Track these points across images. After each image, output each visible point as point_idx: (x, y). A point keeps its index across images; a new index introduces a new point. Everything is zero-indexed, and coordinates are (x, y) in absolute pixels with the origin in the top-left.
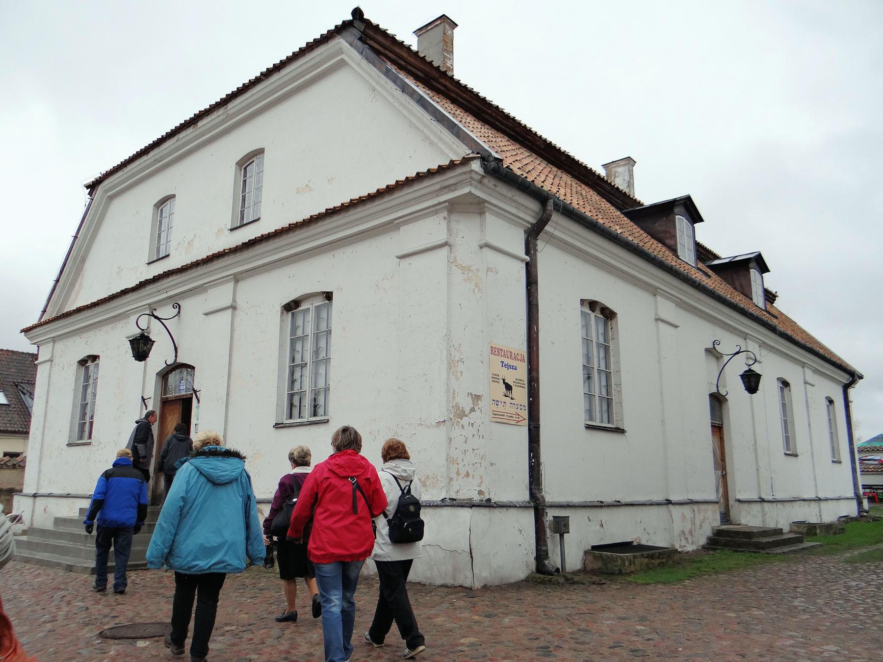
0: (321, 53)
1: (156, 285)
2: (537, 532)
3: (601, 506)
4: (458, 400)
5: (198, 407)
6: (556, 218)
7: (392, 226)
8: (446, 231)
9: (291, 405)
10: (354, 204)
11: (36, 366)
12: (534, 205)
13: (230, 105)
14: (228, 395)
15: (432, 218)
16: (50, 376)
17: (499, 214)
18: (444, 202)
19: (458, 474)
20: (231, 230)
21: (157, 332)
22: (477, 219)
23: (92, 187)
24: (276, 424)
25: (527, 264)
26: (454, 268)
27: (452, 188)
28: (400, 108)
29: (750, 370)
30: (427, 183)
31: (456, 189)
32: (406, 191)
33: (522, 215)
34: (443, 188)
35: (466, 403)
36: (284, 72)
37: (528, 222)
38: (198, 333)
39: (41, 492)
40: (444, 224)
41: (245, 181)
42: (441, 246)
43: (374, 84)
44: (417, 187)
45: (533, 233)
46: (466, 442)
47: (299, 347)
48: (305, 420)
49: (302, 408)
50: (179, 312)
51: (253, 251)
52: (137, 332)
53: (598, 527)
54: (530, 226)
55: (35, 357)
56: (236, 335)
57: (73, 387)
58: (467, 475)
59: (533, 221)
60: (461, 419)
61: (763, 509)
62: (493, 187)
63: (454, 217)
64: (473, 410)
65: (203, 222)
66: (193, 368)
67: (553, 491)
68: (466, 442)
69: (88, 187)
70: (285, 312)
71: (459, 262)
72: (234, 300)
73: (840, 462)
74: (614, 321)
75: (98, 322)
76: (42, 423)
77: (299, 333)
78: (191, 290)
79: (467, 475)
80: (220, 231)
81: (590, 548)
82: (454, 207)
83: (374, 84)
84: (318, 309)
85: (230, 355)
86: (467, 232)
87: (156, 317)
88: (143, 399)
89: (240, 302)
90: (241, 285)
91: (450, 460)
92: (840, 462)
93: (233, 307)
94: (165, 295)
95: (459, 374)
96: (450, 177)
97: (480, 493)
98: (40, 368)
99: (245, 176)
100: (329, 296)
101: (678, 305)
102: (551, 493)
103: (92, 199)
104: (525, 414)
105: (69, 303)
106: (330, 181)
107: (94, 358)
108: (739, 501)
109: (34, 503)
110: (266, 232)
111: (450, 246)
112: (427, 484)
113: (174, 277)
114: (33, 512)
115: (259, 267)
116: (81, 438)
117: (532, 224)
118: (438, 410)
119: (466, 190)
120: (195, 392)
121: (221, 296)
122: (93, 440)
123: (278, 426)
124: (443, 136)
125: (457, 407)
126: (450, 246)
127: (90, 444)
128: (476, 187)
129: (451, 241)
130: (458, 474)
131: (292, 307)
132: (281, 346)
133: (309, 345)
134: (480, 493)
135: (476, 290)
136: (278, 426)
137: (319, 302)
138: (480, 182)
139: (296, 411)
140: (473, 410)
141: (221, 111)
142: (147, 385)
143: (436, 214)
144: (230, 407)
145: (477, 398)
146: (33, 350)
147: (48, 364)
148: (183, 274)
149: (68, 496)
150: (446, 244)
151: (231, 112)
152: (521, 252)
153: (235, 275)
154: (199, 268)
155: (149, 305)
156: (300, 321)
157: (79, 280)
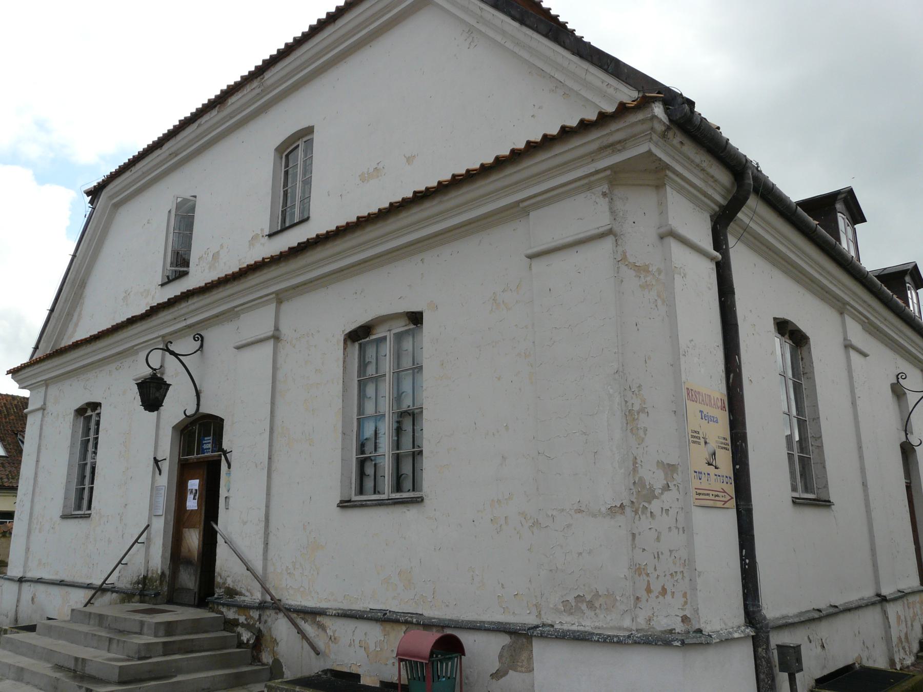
1: (172, 310)
3: (820, 619)
4: (642, 472)
5: (229, 474)
6: (753, 202)
8: (608, 213)
9: (362, 474)
10: (457, 181)
11: (26, 416)
12: (724, 177)
13: (268, 75)
14: (270, 458)
15: (583, 195)
16: (41, 429)
17: (683, 188)
18: (605, 169)
19: (649, 590)
20: (270, 236)
21: (173, 373)
23: (94, 193)
24: (342, 502)
26: (624, 269)
27: (619, 147)
28: (516, 50)
30: (575, 142)
31: (624, 149)
32: (541, 156)
33: (710, 192)
34: (603, 149)
35: (656, 479)
36: (340, 22)
37: (716, 202)
38: (230, 377)
39: (29, 575)
40: (604, 203)
41: (286, 173)
42: (602, 236)
43: (472, 22)
44: (559, 149)
45: (722, 221)
46: (658, 539)
47: (370, 390)
48: (384, 497)
49: (379, 479)
50: (202, 346)
51: (301, 257)
52: (146, 372)
53: (819, 648)
54: (717, 209)
55: (24, 402)
56: (280, 375)
57: (68, 443)
59: (723, 202)
60: (650, 503)
62: (679, 146)
63: (619, 192)
64: (667, 488)
68: (658, 539)
69: (88, 193)
70: (349, 343)
71: (631, 260)
72: (277, 329)
73: (824, 503)
74: (805, 349)
75: (100, 360)
76: (31, 488)
77: (371, 371)
78: (217, 316)
79: (664, 591)
80: (255, 238)
81: (813, 683)
82: (617, 177)
83: (472, 22)
84: (399, 337)
85: (273, 403)
86: (640, 212)
87: (172, 353)
88: (156, 461)
89: (285, 330)
90: (286, 307)
91: (639, 570)
92: (824, 503)
93: (276, 337)
94: (183, 324)
95: (641, 433)
96: (615, 131)
97: (685, 619)
98: (30, 420)
99: (287, 165)
100: (416, 318)
101: (863, 324)
102: (772, 607)
103: (94, 209)
104: (731, 489)
105: (66, 337)
106: (410, 160)
107: (95, 406)
109: (20, 589)
110: (323, 231)
111: (615, 235)
112: (597, 605)
113: (195, 299)
114: (18, 601)
115: (311, 281)
116: (79, 507)
117: (720, 206)
118: (609, 487)
119: (643, 149)
120: (225, 453)
121: (258, 322)
122: (93, 511)
123: (345, 504)
124: (590, 78)
125: (639, 484)
126: (615, 235)
127: (88, 516)
128: (656, 145)
129: (617, 229)
130: (649, 590)
131: (359, 336)
132: (345, 389)
133: (386, 388)
134: (685, 619)
135: (659, 302)
137: (400, 326)
138: (664, 136)
139: (369, 484)
140: (667, 488)
141: (255, 83)
142: (161, 432)
143: (589, 189)
144: (274, 476)
145: (670, 469)
146: (25, 393)
147: (39, 415)
148: (207, 295)
149: (61, 583)
151: (269, 82)
152: (707, 244)
153: (277, 293)
154: (228, 286)
155: (163, 336)
156: (371, 352)
157: (78, 309)
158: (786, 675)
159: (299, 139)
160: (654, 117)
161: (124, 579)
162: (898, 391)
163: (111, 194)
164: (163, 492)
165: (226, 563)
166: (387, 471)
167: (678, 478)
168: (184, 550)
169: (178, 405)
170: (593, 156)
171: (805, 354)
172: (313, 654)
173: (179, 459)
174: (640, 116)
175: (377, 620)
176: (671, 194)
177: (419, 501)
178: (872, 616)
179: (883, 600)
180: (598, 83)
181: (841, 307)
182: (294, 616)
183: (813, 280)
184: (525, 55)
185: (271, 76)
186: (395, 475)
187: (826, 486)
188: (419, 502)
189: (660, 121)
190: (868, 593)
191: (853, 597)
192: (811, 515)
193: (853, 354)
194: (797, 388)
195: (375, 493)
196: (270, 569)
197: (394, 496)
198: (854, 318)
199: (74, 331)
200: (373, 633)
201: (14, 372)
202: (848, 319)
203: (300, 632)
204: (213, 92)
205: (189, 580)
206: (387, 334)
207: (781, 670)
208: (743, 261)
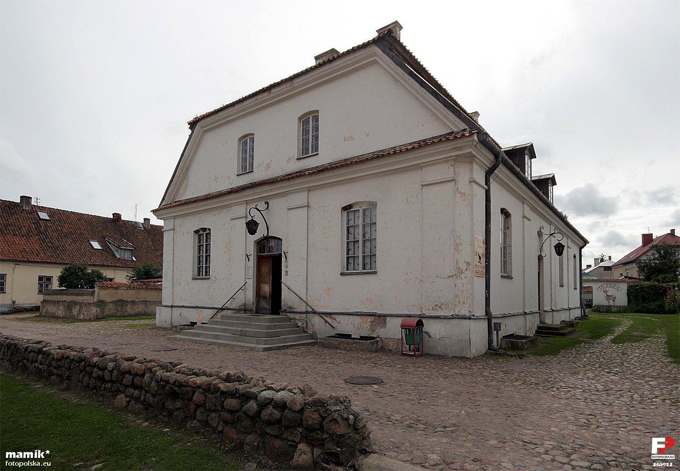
0: (361, 55)
2: (489, 330)
6: (501, 166)
7: (419, 167)
21: (258, 219)
22: (468, 166)
23: (193, 124)
25: (486, 190)
29: (559, 243)
33: (486, 163)
38: (285, 221)
39: (175, 304)
45: (489, 173)
55: (161, 227)
58: (464, 303)
61: (553, 315)
64: (467, 270)
65: (278, 152)
66: (281, 240)
67: (495, 311)
68: (463, 286)
73: (509, 277)
77: (351, 223)
79: (464, 303)
80: (290, 159)
83: (398, 78)
89: (311, 204)
90: (311, 193)
92: (509, 277)
95: (460, 251)
97: (470, 311)
103: (193, 132)
108: (546, 311)
117: (489, 168)
119: (468, 151)
125: (458, 268)
129: (456, 179)
131: (347, 208)
134: (470, 311)
135: (468, 206)
136: (341, 274)
138: (475, 146)
139: (351, 266)
143: (447, 162)
145: (468, 264)
150: (454, 180)
152: (483, 183)
156: (351, 216)
158: (496, 332)
159: (310, 114)
160: (474, 140)
161: (235, 305)
162: (540, 234)
163: (203, 125)
164: (251, 269)
165: (286, 296)
166: (360, 258)
167: (470, 267)
168: (262, 293)
169: (261, 233)
170: (450, 151)
171: (509, 220)
172: (331, 328)
173: (257, 255)
174: (469, 139)
175: (359, 315)
176: (475, 166)
177: (375, 273)
178: (521, 318)
179: (526, 313)
180: (452, 119)
181: (523, 201)
182: (322, 315)
183: (515, 191)
184: (421, 99)
185: (296, 82)
186: (27, 264)
187: (511, 272)
188: (375, 273)
189: (476, 141)
190: (521, 311)
191: (515, 312)
192: (506, 280)
193: (525, 219)
194: (505, 234)
195: (354, 270)
196: (309, 298)
197: (363, 271)
198: (528, 205)
199: (184, 192)
200: (357, 320)
201: (154, 211)
202: (525, 205)
203: (326, 321)
204: (265, 85)
205: (265, 304)
206: (360, 209)
207: (495, 330)
208: (494, 186)
